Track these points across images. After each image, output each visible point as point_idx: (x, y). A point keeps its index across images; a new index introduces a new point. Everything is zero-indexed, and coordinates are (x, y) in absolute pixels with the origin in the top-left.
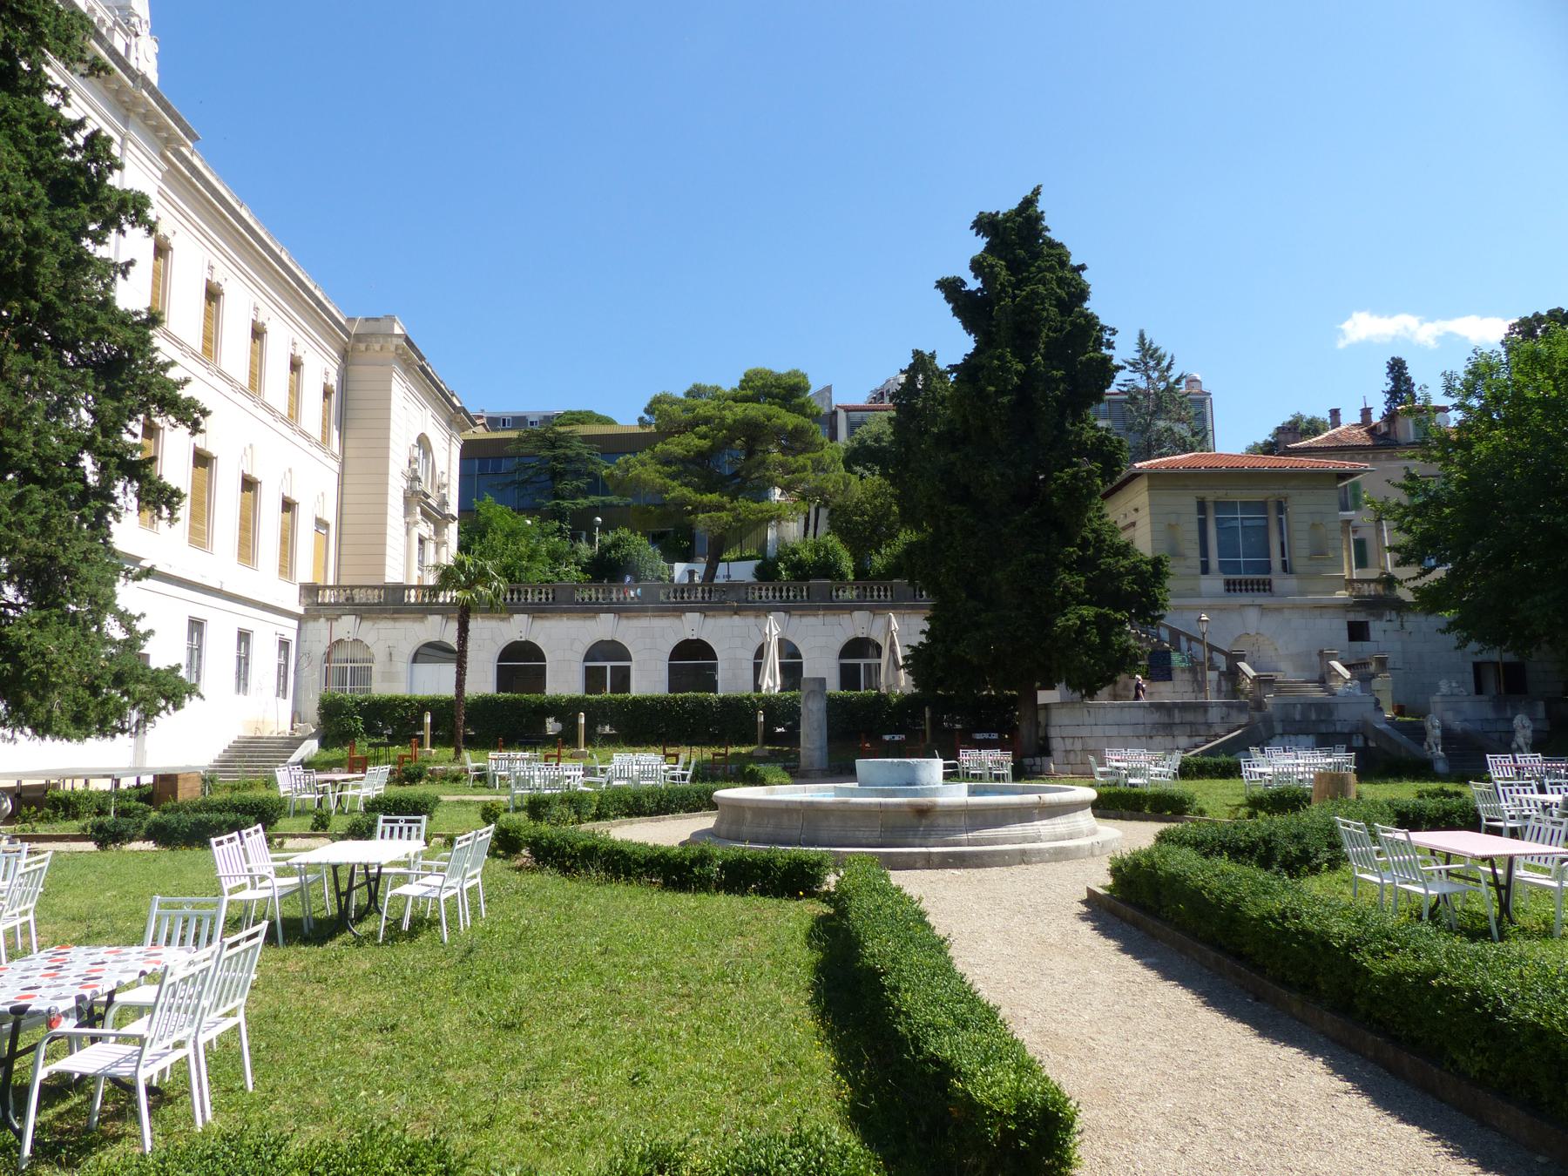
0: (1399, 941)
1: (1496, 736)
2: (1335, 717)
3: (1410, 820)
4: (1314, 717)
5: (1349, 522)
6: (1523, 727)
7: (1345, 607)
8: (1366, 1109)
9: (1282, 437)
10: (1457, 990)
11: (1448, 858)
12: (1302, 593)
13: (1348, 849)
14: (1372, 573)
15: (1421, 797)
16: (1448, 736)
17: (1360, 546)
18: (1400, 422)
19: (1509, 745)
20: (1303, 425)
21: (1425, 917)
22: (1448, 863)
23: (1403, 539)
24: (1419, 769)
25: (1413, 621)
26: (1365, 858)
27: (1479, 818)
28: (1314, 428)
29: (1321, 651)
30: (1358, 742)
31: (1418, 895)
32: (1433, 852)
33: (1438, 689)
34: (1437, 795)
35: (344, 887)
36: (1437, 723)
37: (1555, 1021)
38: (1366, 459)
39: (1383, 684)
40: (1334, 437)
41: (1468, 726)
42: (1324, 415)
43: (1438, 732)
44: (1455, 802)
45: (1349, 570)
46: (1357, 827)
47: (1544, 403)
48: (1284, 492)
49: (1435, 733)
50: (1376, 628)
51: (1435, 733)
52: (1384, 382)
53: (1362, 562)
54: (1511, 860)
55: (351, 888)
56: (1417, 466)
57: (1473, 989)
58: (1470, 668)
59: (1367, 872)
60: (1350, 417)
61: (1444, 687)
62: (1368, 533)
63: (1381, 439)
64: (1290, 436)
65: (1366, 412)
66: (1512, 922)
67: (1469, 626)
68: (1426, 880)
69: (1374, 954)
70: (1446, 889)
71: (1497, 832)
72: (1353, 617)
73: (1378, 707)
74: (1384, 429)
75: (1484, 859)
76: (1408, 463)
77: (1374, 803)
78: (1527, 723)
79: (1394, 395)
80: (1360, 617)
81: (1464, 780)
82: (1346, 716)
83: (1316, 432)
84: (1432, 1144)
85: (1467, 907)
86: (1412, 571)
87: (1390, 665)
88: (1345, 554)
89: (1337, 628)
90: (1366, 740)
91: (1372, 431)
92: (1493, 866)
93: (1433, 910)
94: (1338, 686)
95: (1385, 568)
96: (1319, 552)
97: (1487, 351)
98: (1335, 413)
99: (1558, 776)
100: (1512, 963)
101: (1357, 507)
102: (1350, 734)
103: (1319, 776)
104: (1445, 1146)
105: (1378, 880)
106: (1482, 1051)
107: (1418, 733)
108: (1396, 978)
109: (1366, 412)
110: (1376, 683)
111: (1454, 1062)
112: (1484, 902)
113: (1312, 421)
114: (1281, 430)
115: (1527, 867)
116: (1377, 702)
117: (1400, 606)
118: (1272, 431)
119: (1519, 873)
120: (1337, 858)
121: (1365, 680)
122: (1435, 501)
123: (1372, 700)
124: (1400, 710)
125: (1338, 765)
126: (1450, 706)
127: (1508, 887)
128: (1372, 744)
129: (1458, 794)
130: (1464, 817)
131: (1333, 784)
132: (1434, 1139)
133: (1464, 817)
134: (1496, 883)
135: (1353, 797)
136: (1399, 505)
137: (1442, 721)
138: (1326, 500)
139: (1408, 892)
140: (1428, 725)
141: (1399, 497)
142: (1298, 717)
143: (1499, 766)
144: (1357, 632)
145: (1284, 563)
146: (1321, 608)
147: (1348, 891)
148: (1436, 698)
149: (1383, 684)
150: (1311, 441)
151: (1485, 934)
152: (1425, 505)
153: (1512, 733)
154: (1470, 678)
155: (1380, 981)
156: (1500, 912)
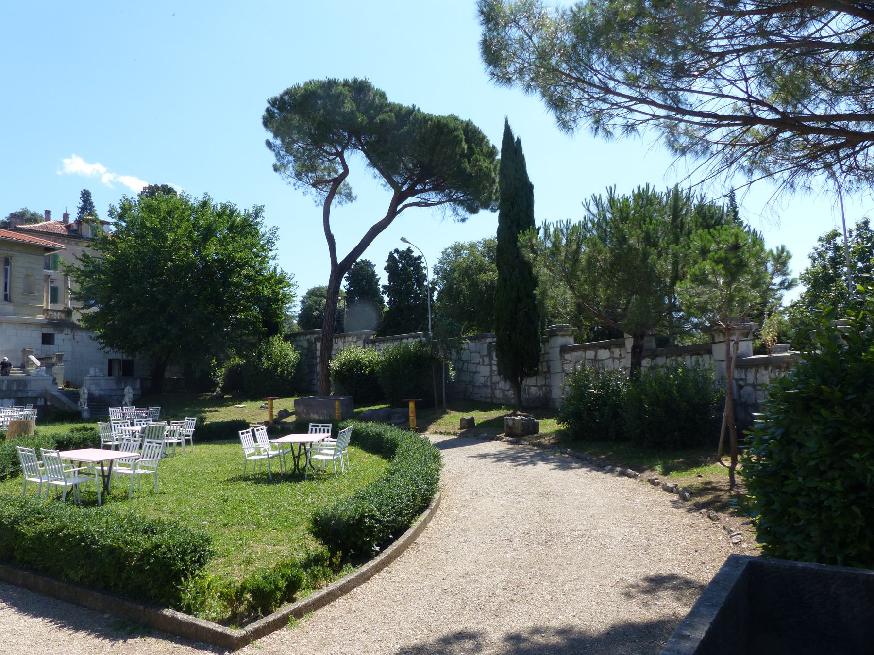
0: (45, 514)
1: (116, 398)
2: (29, 388)
3: (63, 445)
4: (15, 388)
5: (49, 276)
6: (129, 392)
7: (42, 325)
8: (13, 616)
9: (13, 220)
10: (73, 536)
11: (80, 464)
12: (15, 315)
13: (23, 465)
14: (60, 307)
15: (72, 432)
16: (91, 398)
17: (54, 291)
18: (85, 225)
19: (121, 402)
20: (28, 216)
21: (63, 499)
22: (80, 466)
23: (77, 287)
24: (74, 417)
25: (79, 335)
26: (33, 469)
27: (100, 441)
28: (34, 219)
29: (24, 350)
30: (41, 402)
31: (62, 486)
32: (72, 462)
33: (88, 372)
34: (81, 430)
35: (296, 453)
36: (86, 391)
37: (120, 543)
38: (63, 242)
39: (59, 370)
40: (46, 226)
41: (102, 393)
42: (42, 213)
43: (86, 396)
44: (89, 433)
45: (46, 304)
46: (23, 451)
47: (153, 229)
48: (10, 253)
49: (84, 397)
50: (59, 337)
51: (84, 397)
52: (78, 202)
53: (54, 300)
54: (111, 462)
55: (299, 455)
56: (90, 252)
57: (81, 533)
58: (107, 362)
59: (33, 477)
60: (57, 217)
61: (92, 371)
62: (59, 284)
63: (73, 233)
64: (19, 221)
65: (66, 216)
66: (109, 494)
67: (110, 339)
68: (66, 477)
69: (28, 524)
70: (77, 481)
71: (108, 448)
72: (45, 330)
73: (55, 382)
74: (75, 227)
75: (98, 463)
76: (86, 249)
77: (44, 437)
78: (131, 390)
79: (83, 209)
80: (50, 331)
81: (95, 421)
82: (35, 388)
83: (36, 221)
84: (49, 624)
85: (88, 489)
86: (79, 305)
87: (64, 358)
88: (45, 294)
89: (37, 336)
90: (46, 401)
91: (68, 227)
92: (102, 466)
93: (68, 494)
94: (32, 370)
95: (67, 305)
96: (29, 291)
97: (129, 198)
98: (48, 213)
99: (142, 417)
100: (103, 516)
101: (55, 268)
102: (37, 398)
103: (12, 423)
104: (56, 624)
105: (39, 481)
106: (83, 566)
107: (75, 397)
108: (40, 535)
109: (66, 216)
110: (55, 369)
111: (67, 576)
112: (96, 486)
113: (33, 215)
114: (13, 216)
115: (120, 465)
116: (55, 380)
117: (74, 327)
118: (8, 215)
119: (116, 468)
120: (17, 471)
121: (49, 367)
122: (97, 270)
123: (52, 378)
124: (67, 384)
125: (27, 416)
126: (95, 381)
127: (108, 476)
128: (49, 403)
129: (92, 429)
130: (93, 441)
131: (21, 427)
132: (51, 622)
133: (93, 441)
134: (103, 476)
135: (32, 434)
136: (78, 269)
137: (89, 390)
138: (37, 262)
139: (56, 486)
140: (81, 392)
141: (79, 264)
142: (4, 388)
143: (114, 413)
144: (47, 339)
145: (6, 295)
146: (27, 324)
147: (21, 489)
148: (87, 378)
149: (59, 370)
150: (32, 226)
151: (94, 503)
152: (92, 272)
153: (123, 396)
154: (106, 367)
155: (31, 539)
156: (104, 489)
